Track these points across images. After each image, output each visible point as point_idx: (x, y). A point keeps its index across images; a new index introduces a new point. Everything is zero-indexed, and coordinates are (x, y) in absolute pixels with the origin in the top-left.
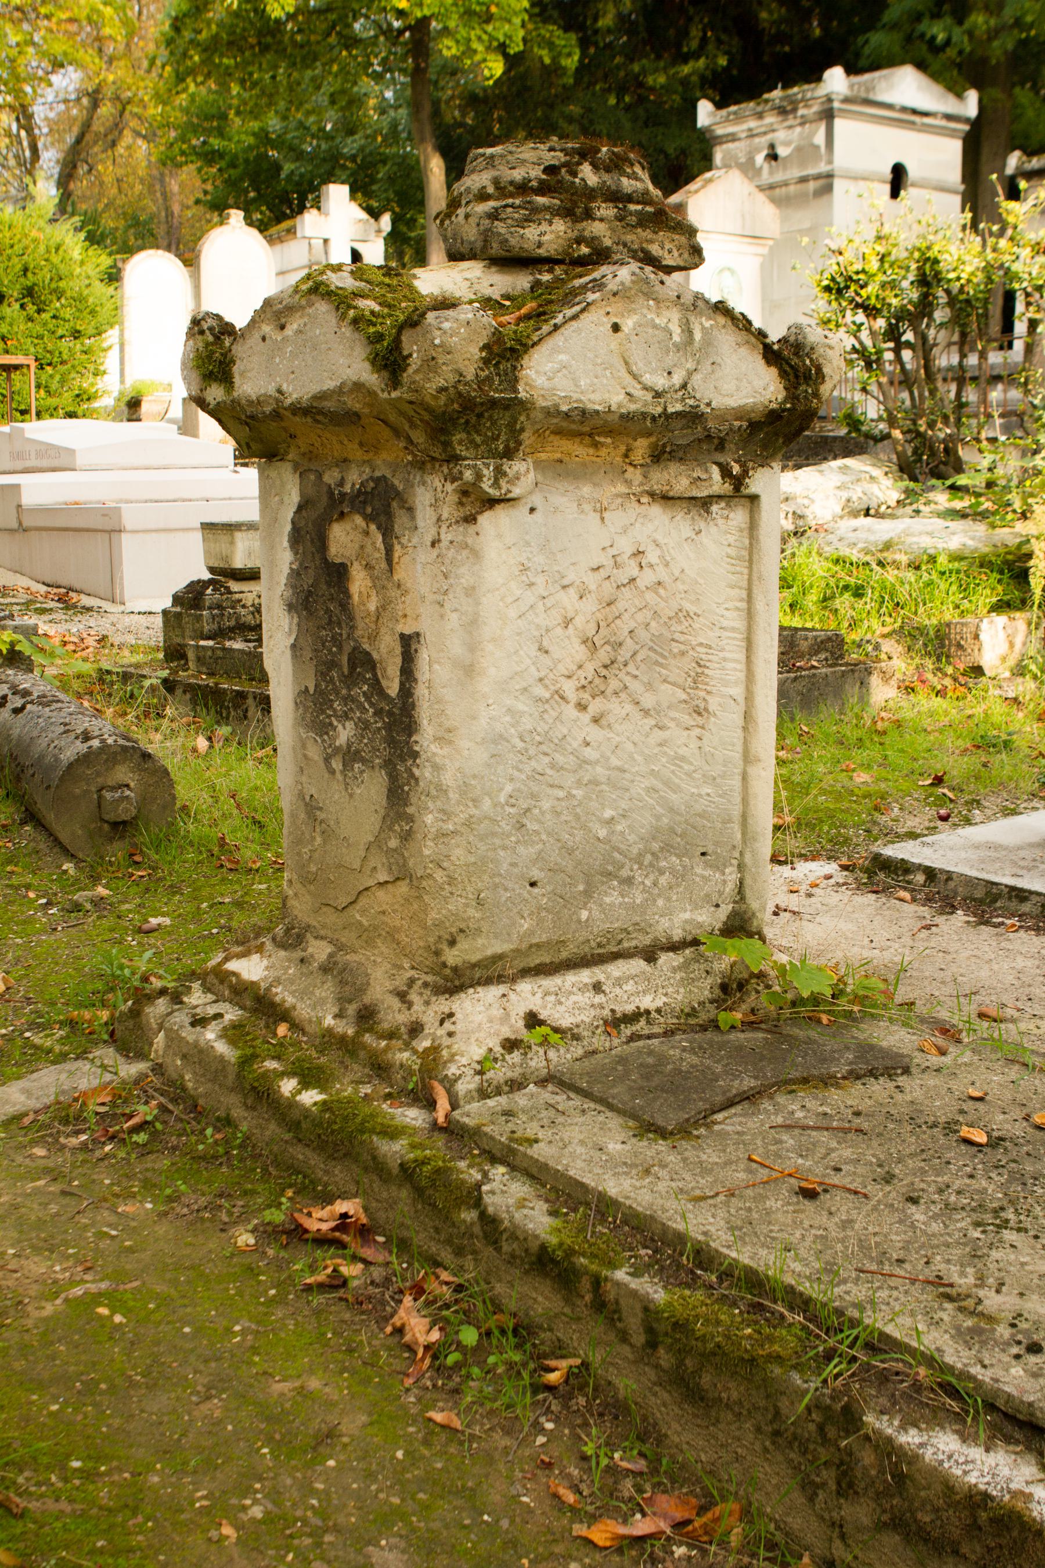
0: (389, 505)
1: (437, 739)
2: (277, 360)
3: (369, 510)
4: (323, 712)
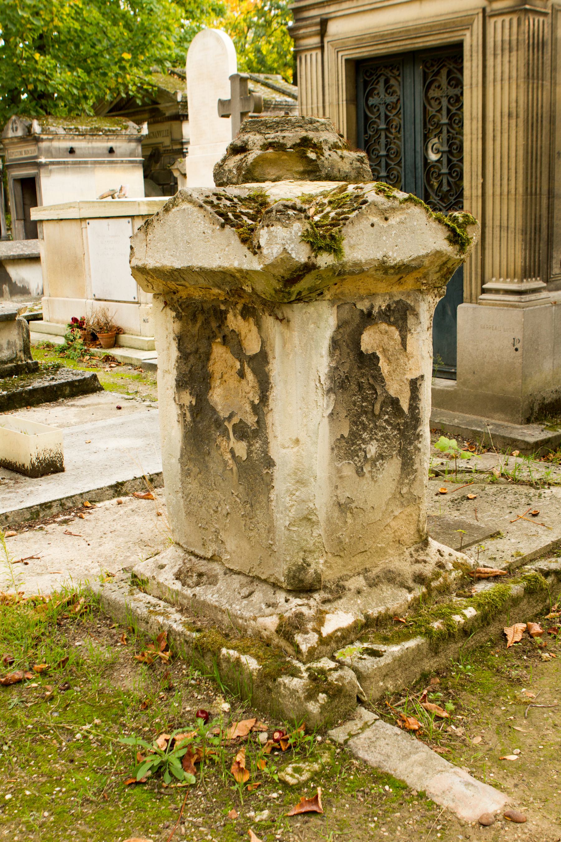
2: (384, 238)
3: (392, 319)
4: (353, 444)
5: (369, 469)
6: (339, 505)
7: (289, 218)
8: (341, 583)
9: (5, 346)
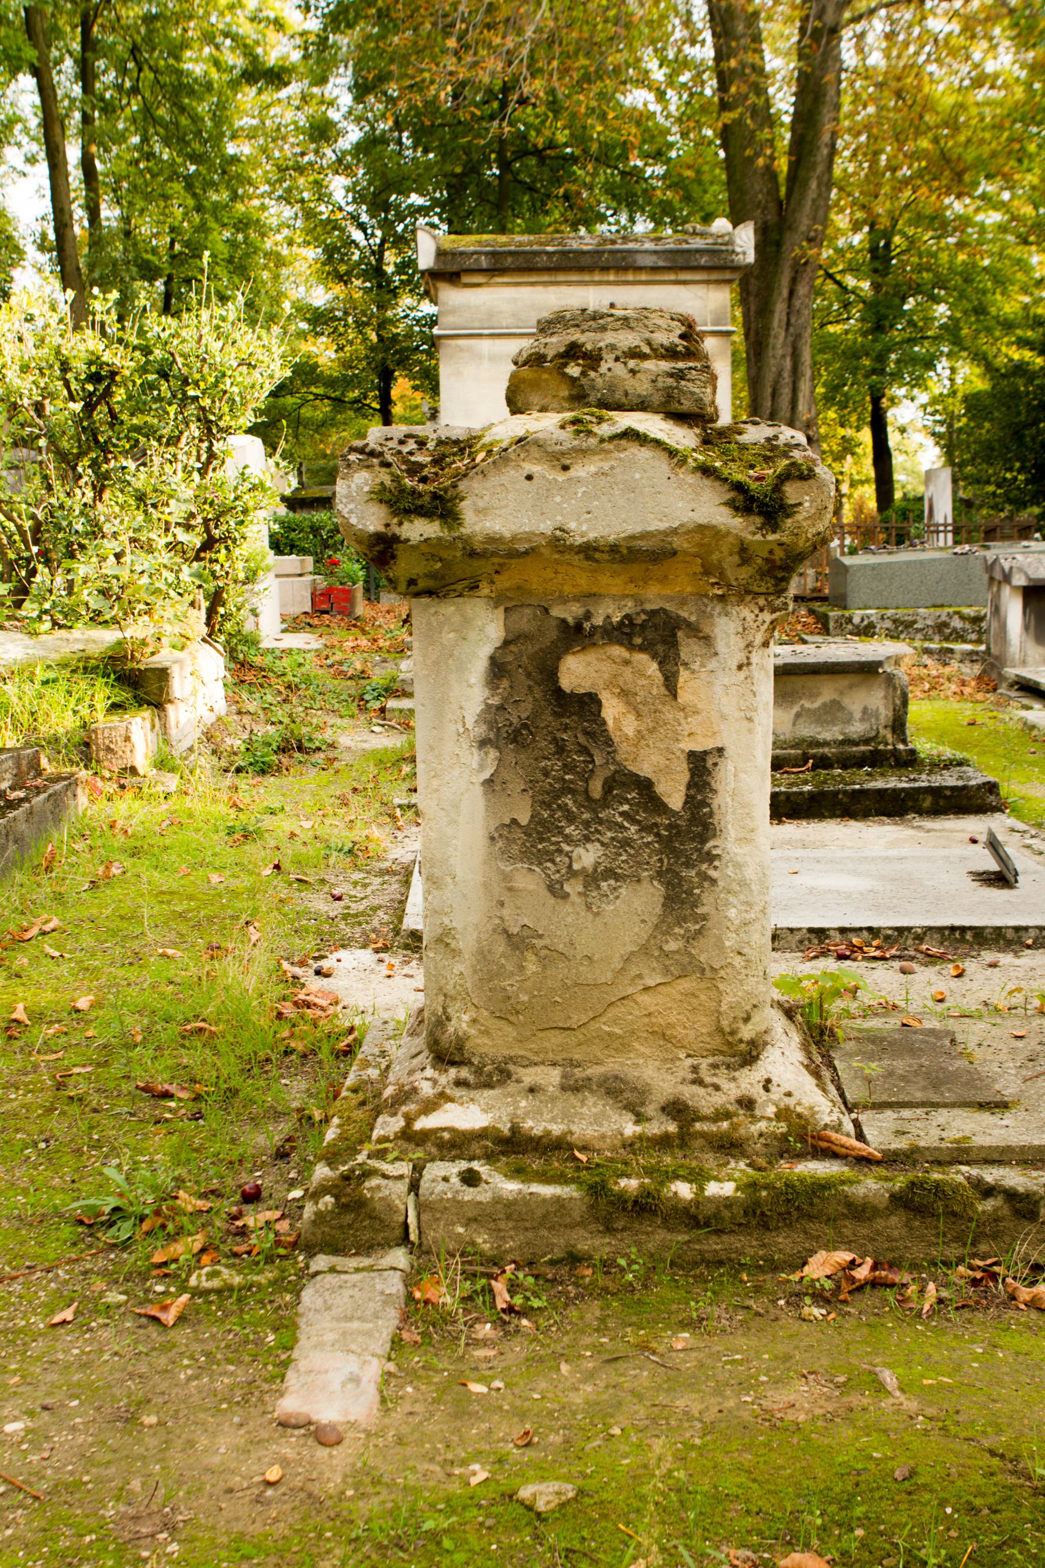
0: (675, 635)
1: (739, 840)
2: (558, 499)
4: (542, 840)
5: (580, 889)
6: (509, 936)
7: (349, 466)
8: (511, 1067)
9: (858, 715)
